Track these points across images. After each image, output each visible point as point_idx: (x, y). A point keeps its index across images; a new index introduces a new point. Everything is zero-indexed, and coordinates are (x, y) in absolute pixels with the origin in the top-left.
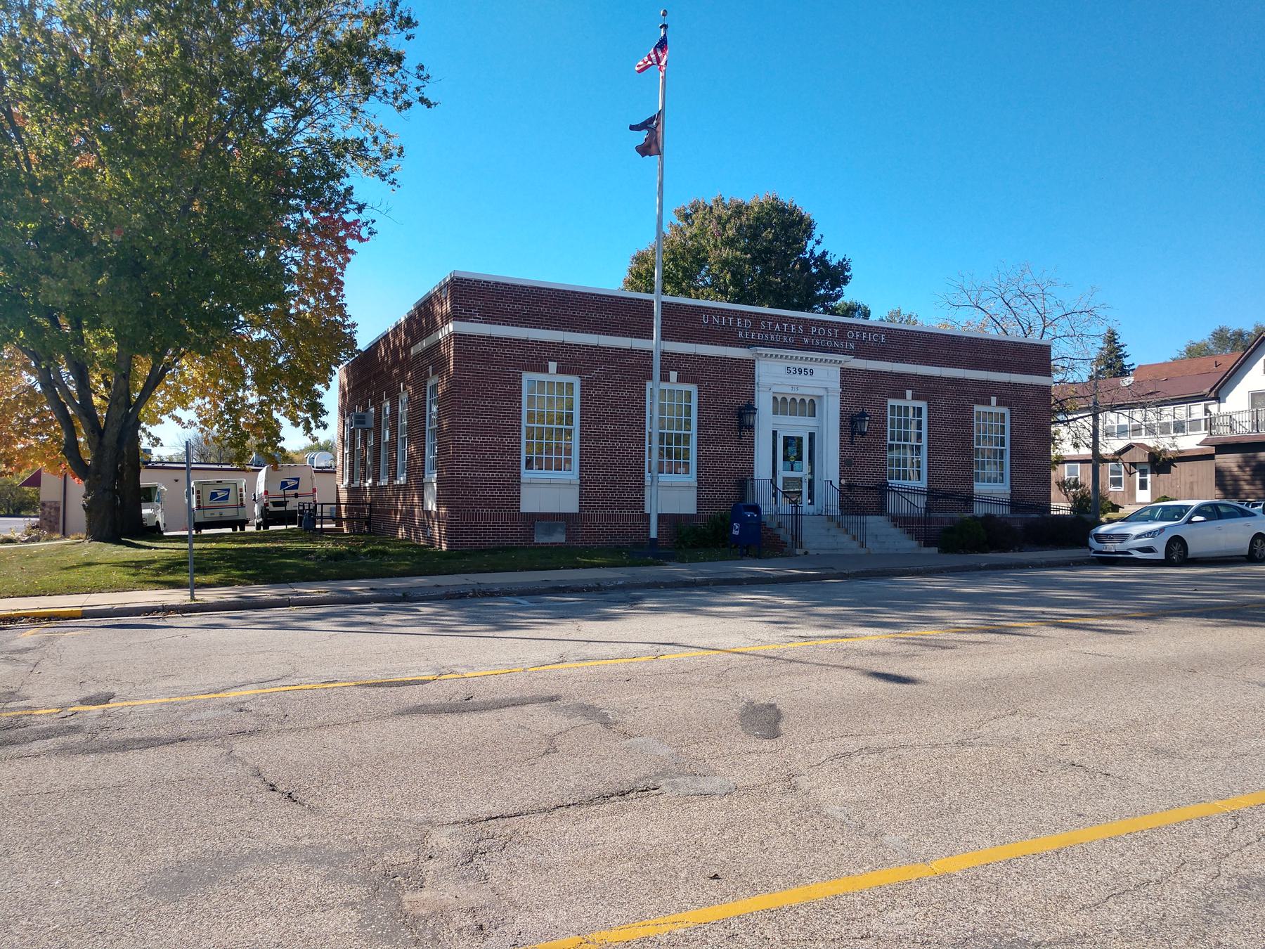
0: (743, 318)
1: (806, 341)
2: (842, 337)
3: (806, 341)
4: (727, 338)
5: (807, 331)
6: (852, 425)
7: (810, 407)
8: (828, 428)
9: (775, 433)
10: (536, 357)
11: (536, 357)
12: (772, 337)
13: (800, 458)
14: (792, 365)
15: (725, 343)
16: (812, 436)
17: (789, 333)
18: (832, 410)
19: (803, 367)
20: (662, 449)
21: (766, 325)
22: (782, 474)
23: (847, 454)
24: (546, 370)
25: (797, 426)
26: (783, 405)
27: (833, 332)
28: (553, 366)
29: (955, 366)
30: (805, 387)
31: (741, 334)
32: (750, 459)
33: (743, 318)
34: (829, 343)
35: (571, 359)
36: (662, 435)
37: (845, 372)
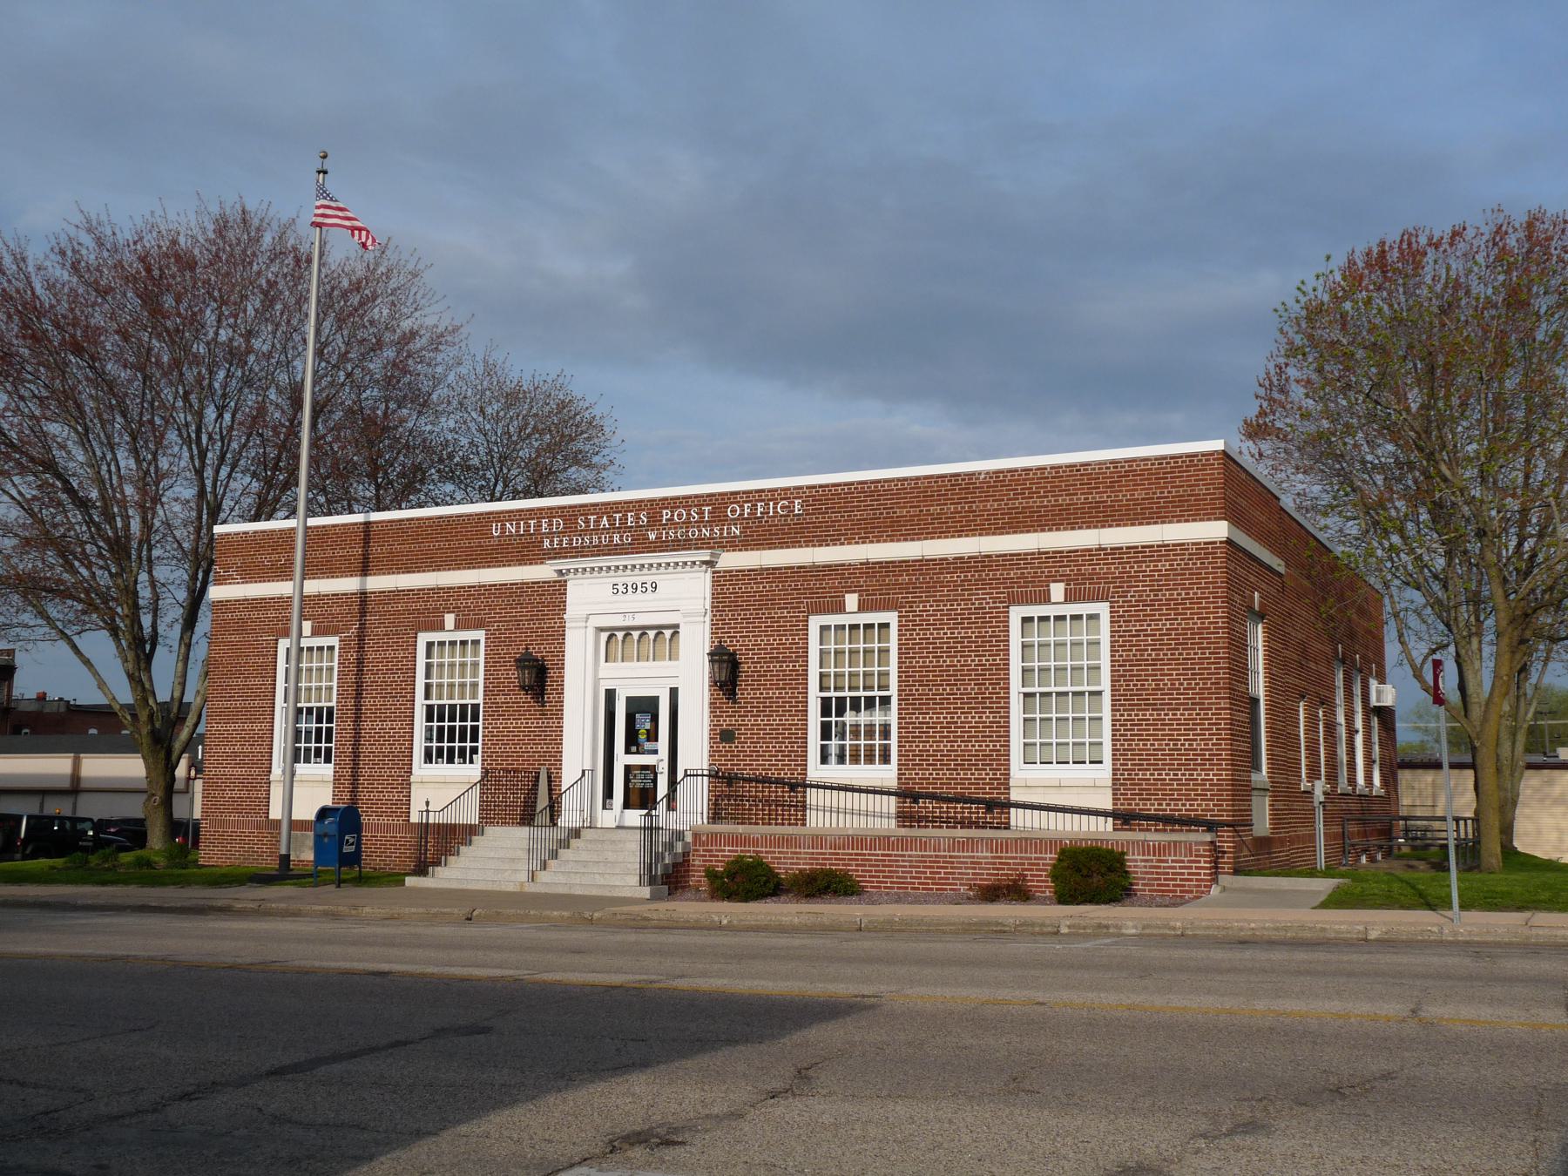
0: (550, 518)
1: (652, 536)
2: (719, 517)
3: (652, 536)
4: (528, 551)
5: (654, 520)
6: (727, 672)
7: (663, 637)
8: (688, 675)
9: (610, 695)
10: (1027, 579)
11: (1027, 579)
12: (596, 541)
13: (653, 735)
14: (620, 581)
15: (522, 561)
16: (674, 693)
17: (623, 525)
18: (696, 643)
19: (638, 580)
20: (429, 729)
21: (587, 522)
22: (622, 759)
23: (553, 723)
24: (1045, 599)
25: (637, 678)
26: (621, 640)
27: (701, 513)
28: (1057, 590)
29: (960, 533)
30: (643, 609)
31: (547, 543)
32: (554, 739)
33: (550, 518)
34: (693, 533)
35: (879, 584)
36: (430, 708)
37: (723, 581)
